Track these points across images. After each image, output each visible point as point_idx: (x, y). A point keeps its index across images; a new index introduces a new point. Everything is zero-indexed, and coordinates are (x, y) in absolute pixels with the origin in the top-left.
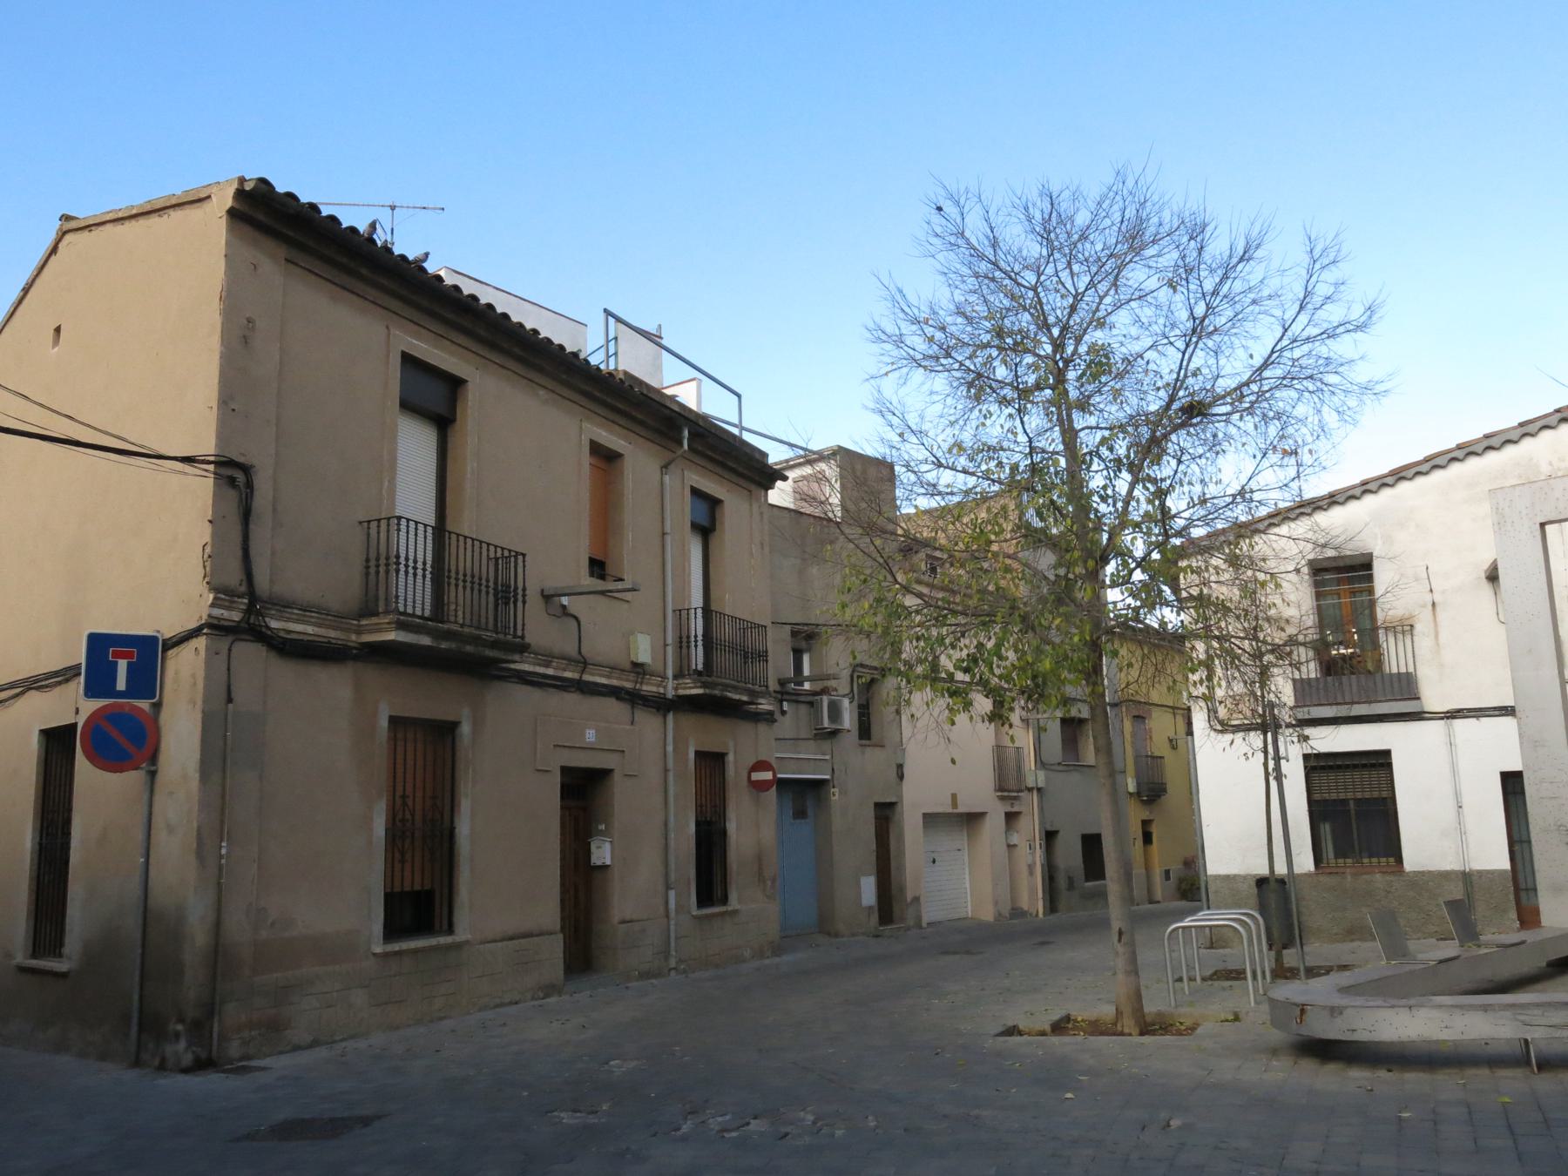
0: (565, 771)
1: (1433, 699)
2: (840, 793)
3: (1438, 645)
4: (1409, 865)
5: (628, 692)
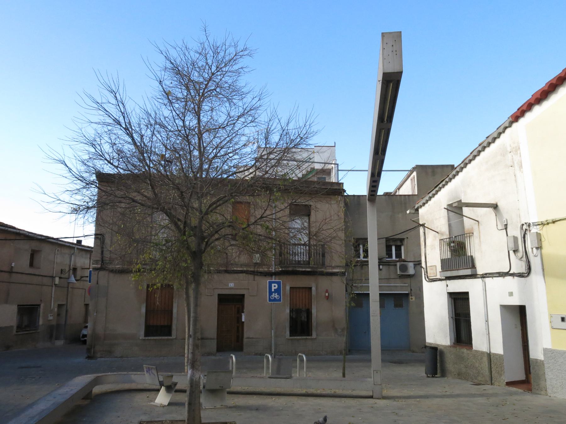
0: (219, 295)
1: (480, 270)
2: (416, 298)
3: (480, 242)
4: (474, 348)
5: (251, 271)
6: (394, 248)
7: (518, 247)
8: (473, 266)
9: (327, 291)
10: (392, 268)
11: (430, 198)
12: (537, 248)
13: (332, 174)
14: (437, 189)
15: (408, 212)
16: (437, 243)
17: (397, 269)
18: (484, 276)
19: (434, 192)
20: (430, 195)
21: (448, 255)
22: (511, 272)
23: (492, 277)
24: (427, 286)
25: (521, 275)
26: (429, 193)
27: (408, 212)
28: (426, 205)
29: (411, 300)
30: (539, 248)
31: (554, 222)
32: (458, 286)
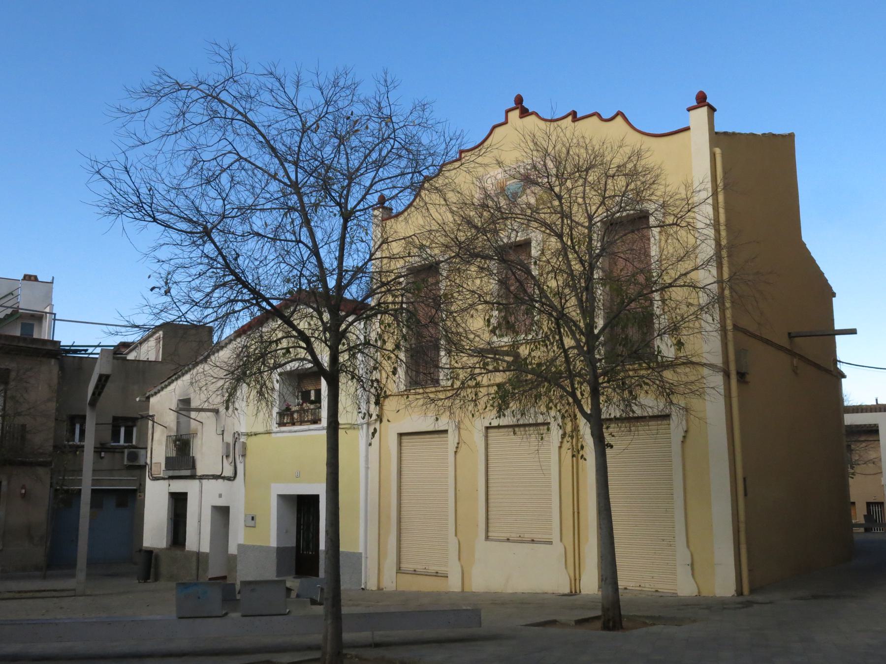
4: (187, 549)
6: (123, 430)
7: (230, 453)
8: (193, 467)
9: (24, 487)
10: (117, 456)
11: (162, 389)
12: (242, 456)
13: (44, 321)
14: (169, 380)
15: (138, 399)
16: (164, 439)
17: (123, 458)
18: (202, 477)
19: (166, 383)
20: (163, 385)
21: (173, 454)
22: (223, 475)
23: (208, 479)
24: (149, 484)
25: (229, 479)
26: (161, 383)
27: (138, 399)
28: (158, 395)
29: (139, 498)
30: (244, 456)
31: (256, 434)
32: (178, 486)
